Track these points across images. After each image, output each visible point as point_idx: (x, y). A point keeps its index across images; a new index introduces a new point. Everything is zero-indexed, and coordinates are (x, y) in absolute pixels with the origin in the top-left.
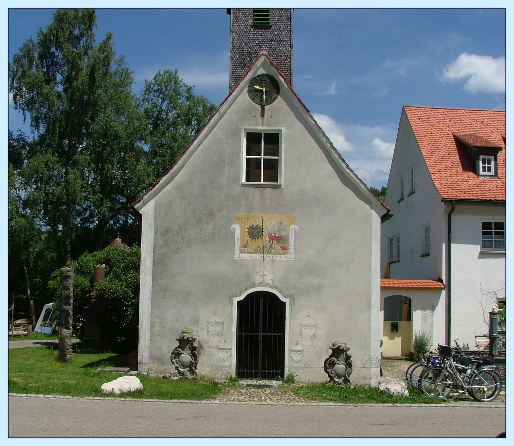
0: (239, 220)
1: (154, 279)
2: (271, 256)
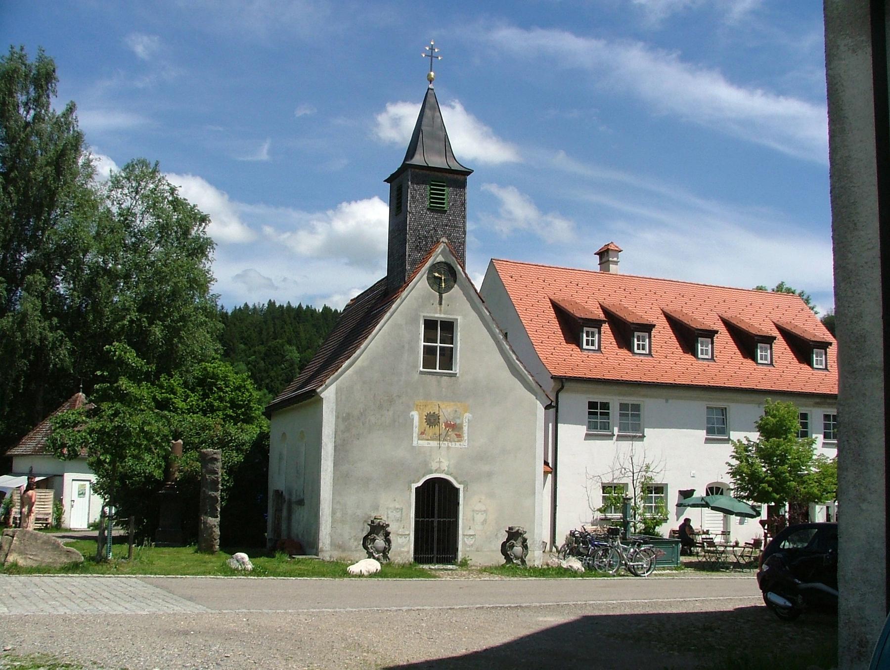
0: (417, 407)
1: (336, 464)
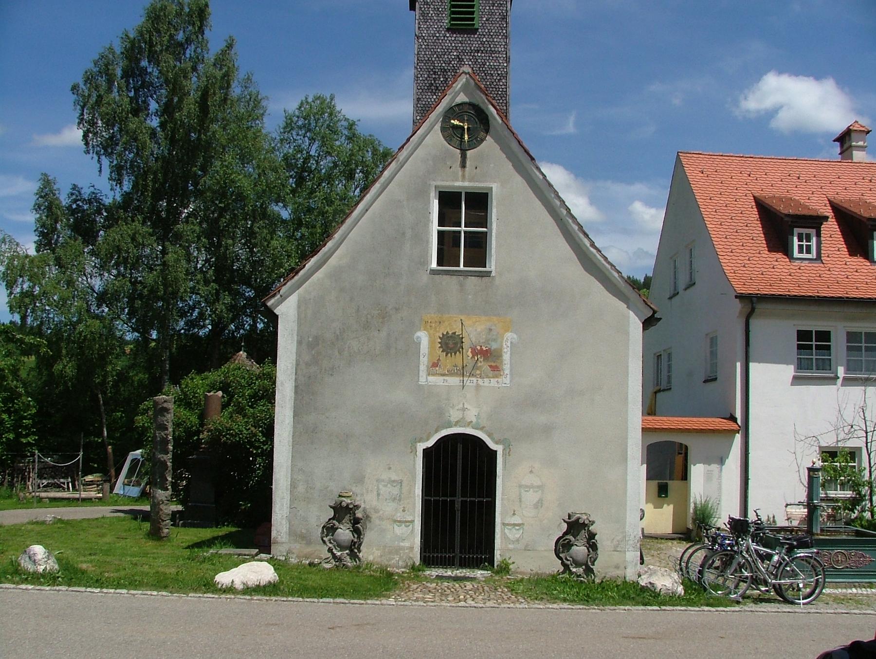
0: (426, 325)
2: (475, 379)
